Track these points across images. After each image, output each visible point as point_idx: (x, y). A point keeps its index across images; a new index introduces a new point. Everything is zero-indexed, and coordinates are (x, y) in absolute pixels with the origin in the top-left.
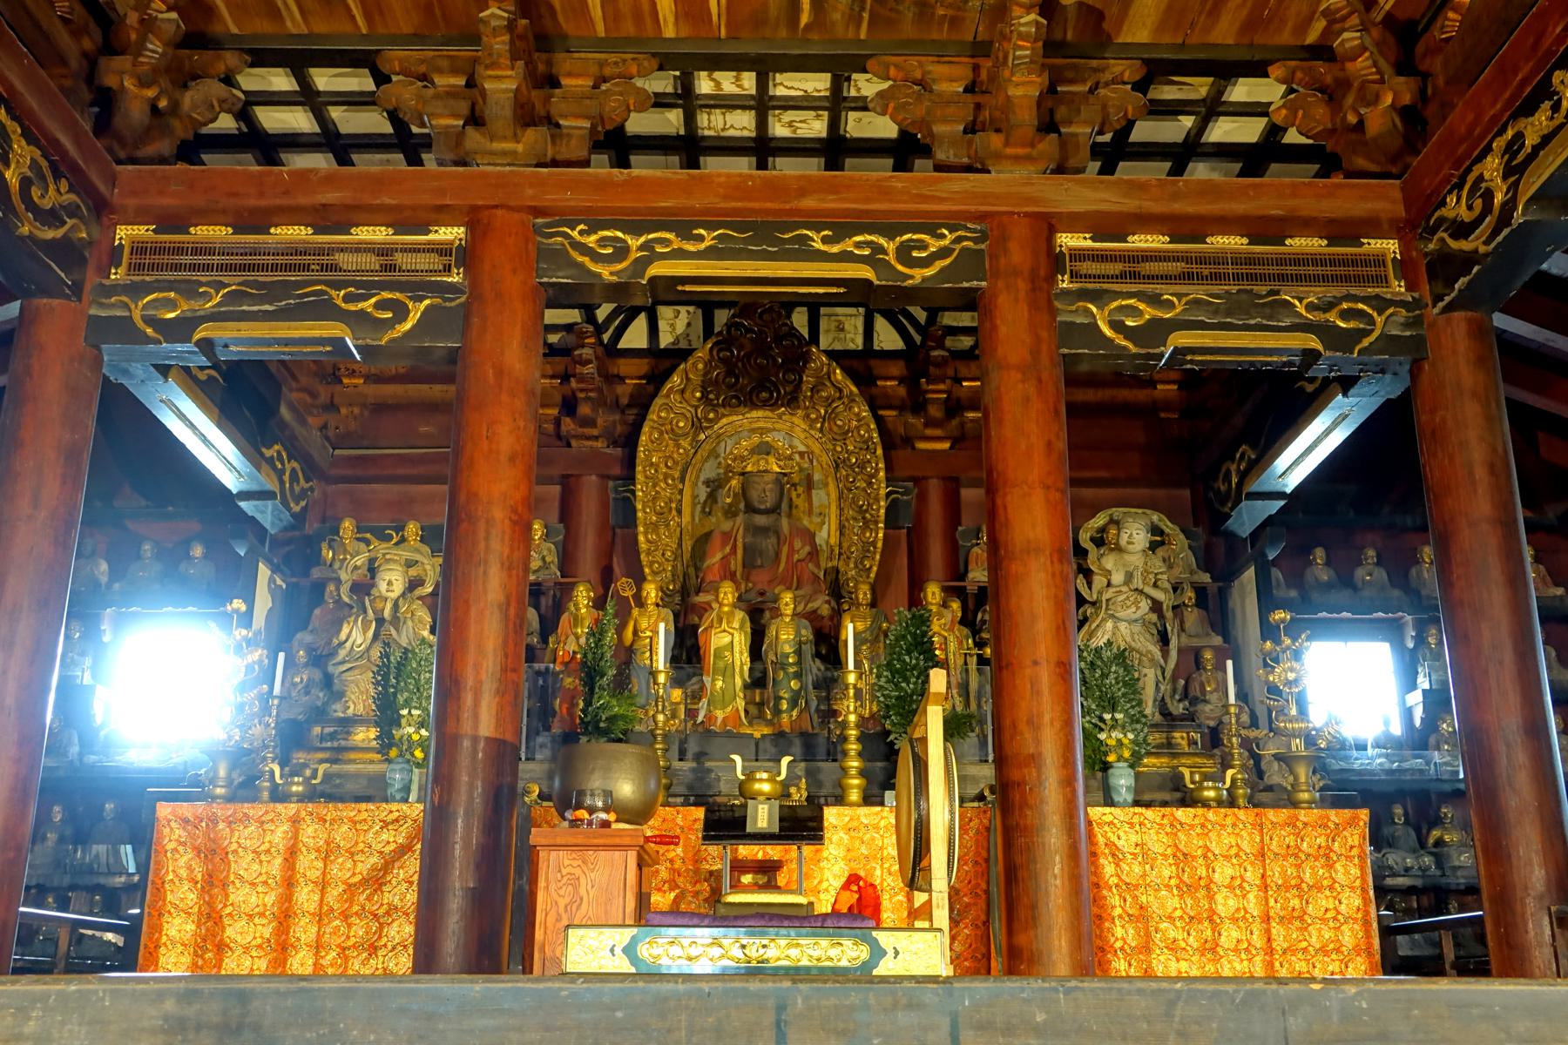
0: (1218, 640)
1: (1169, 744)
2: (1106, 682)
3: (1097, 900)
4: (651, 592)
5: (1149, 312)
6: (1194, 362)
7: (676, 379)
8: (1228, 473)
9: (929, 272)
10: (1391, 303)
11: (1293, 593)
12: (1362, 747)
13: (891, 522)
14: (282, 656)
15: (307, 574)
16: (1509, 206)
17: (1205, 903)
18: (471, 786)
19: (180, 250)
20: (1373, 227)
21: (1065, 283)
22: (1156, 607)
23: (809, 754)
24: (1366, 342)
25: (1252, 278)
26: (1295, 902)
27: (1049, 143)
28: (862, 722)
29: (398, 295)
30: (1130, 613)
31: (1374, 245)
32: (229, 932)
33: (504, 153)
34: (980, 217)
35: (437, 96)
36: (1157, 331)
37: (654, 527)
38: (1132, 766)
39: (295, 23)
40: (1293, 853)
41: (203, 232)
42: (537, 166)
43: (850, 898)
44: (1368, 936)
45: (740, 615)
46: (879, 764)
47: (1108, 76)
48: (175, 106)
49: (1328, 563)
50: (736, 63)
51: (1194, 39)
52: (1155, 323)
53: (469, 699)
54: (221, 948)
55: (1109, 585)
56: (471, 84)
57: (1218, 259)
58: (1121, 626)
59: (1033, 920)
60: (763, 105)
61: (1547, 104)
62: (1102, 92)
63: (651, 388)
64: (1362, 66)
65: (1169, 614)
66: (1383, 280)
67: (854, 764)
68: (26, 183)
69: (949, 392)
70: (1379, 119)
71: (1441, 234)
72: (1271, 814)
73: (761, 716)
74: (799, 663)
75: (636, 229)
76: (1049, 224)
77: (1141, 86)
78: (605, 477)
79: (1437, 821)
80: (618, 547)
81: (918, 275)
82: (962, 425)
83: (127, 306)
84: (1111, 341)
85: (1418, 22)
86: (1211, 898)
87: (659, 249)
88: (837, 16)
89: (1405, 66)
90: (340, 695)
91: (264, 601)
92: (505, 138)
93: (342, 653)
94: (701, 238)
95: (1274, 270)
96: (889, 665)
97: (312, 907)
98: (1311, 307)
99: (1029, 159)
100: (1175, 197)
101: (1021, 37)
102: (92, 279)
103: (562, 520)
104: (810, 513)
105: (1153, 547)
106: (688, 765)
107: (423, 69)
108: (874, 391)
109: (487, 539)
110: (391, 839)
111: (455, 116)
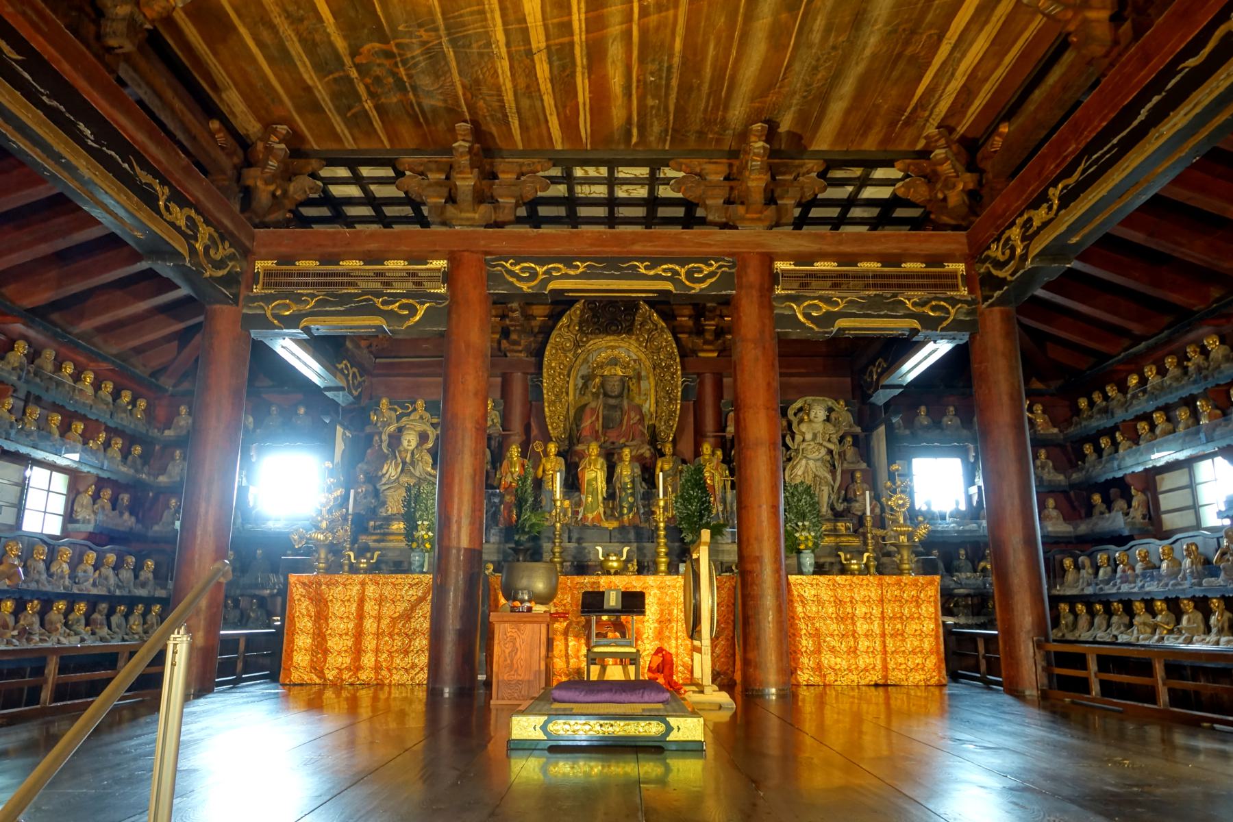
0: (864, 466)
1: (835, 530)
2: (799, 503)
3: (793, 625)
4: (552, 448)
5: (825, 308)
6: (848, 334)
7: (564, 319)
8: (871, 372)
9: (704, 286)
10: (960, 301)
11: (907, 432)
12: (943, 517)
13: (684, 397)
14: (352, 492)
15: (363, 430)
16: (1024, 257)
17: (850, 627)
18: (457, 575)
19: (291, 275)
20: (952, 258)
21: (779, 291)
22: (830, 452)
23: (639, 537)
24: (945, 324)
25: (883, 286)
26: (899, 626)
27: (770, 212)
28: (668, 521)
29: (411, 301)
30: (815, 455)
31: (951, 266)
32: (330, 643)
33: (468, 219)
34: (731, 255)
35: (430, 185)
36: (829, 318)
37: (552, 403)
38: (813, 551)
39: (349, 144)
40: (899, 600)
41: (302, 264)
42: (487, 226)
43: (658, 659)
44: (937, 644)
45: (601, 460)
46: (677, 544)
47: (804, 170)
48: (285, 192)
49: (927, 415)
50: (597, 163)
51: (853, 149)
52: (828, 313)
53: (455, 527)
54: (326, 652)
55: (804, 440)
56: (448, 178)
57: (863, 276)
58: (809, 466)
59: (757, 645)
60: (611, 182)
61: (1045, 205)
62: (801, 179)
63: (551, 323)
64: (947, 168)
65: (836, 457)
66: (955, 287)
67: (662, 541)
68: (207, 249)
69: (717, 326)
70: (955, 198)
71: (987, 265)
72: (887, 579)
73: (613, 515)
74: (633, 488)
75: (541, 261)
76: (770, 258)
77: (822, 175)
78: (525, 374)
79: (983, 558)
80: (534, 410)
81: (698, 287)
82: (724, 342)
83: (262, 308)
84: (803, 324)
85: (978, 140)
86: (854, 624)
87: (554, 274)
88: (652, 138)
89: (971, 167)
90: (384, 504)
91: (340, 446)
92: (468, 211)
93: (384, 480)
94: (578, 267)
95: (895, 281)
96: (682, 496)
97: (374, 630)
98: (914, 304)
99: (759, 219)
100: (840, 243)
101: (755, 154)
102: (244, 293)
103: (503, 397)
104: (640, 393)
105: (828, 419)
106: (572, 545)
107: (422, 168)
108: (675, 323)
109: (463, 439)
110: (414, 593)
111: (441, 197)
